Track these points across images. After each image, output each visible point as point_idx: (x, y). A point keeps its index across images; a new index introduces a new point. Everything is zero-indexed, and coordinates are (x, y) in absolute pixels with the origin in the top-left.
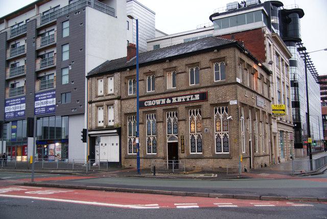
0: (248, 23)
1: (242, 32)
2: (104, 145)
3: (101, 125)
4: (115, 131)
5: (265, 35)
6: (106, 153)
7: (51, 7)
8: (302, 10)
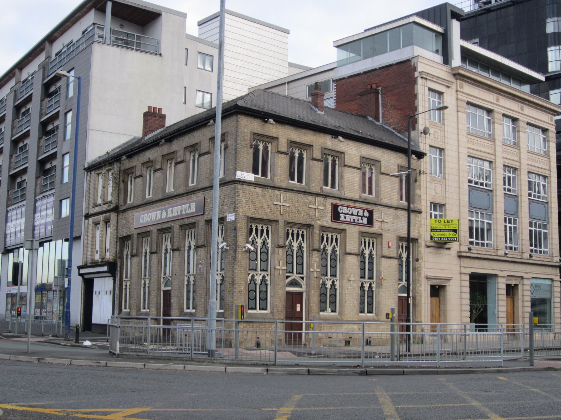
0: (390, 51)
1: (381, 68)
2: (97, 293)
3: (97, 257)
4: (105, 268)
5: (416, 74)
6: (188, 335)
7: (29, 73)
8: (145, 115)
